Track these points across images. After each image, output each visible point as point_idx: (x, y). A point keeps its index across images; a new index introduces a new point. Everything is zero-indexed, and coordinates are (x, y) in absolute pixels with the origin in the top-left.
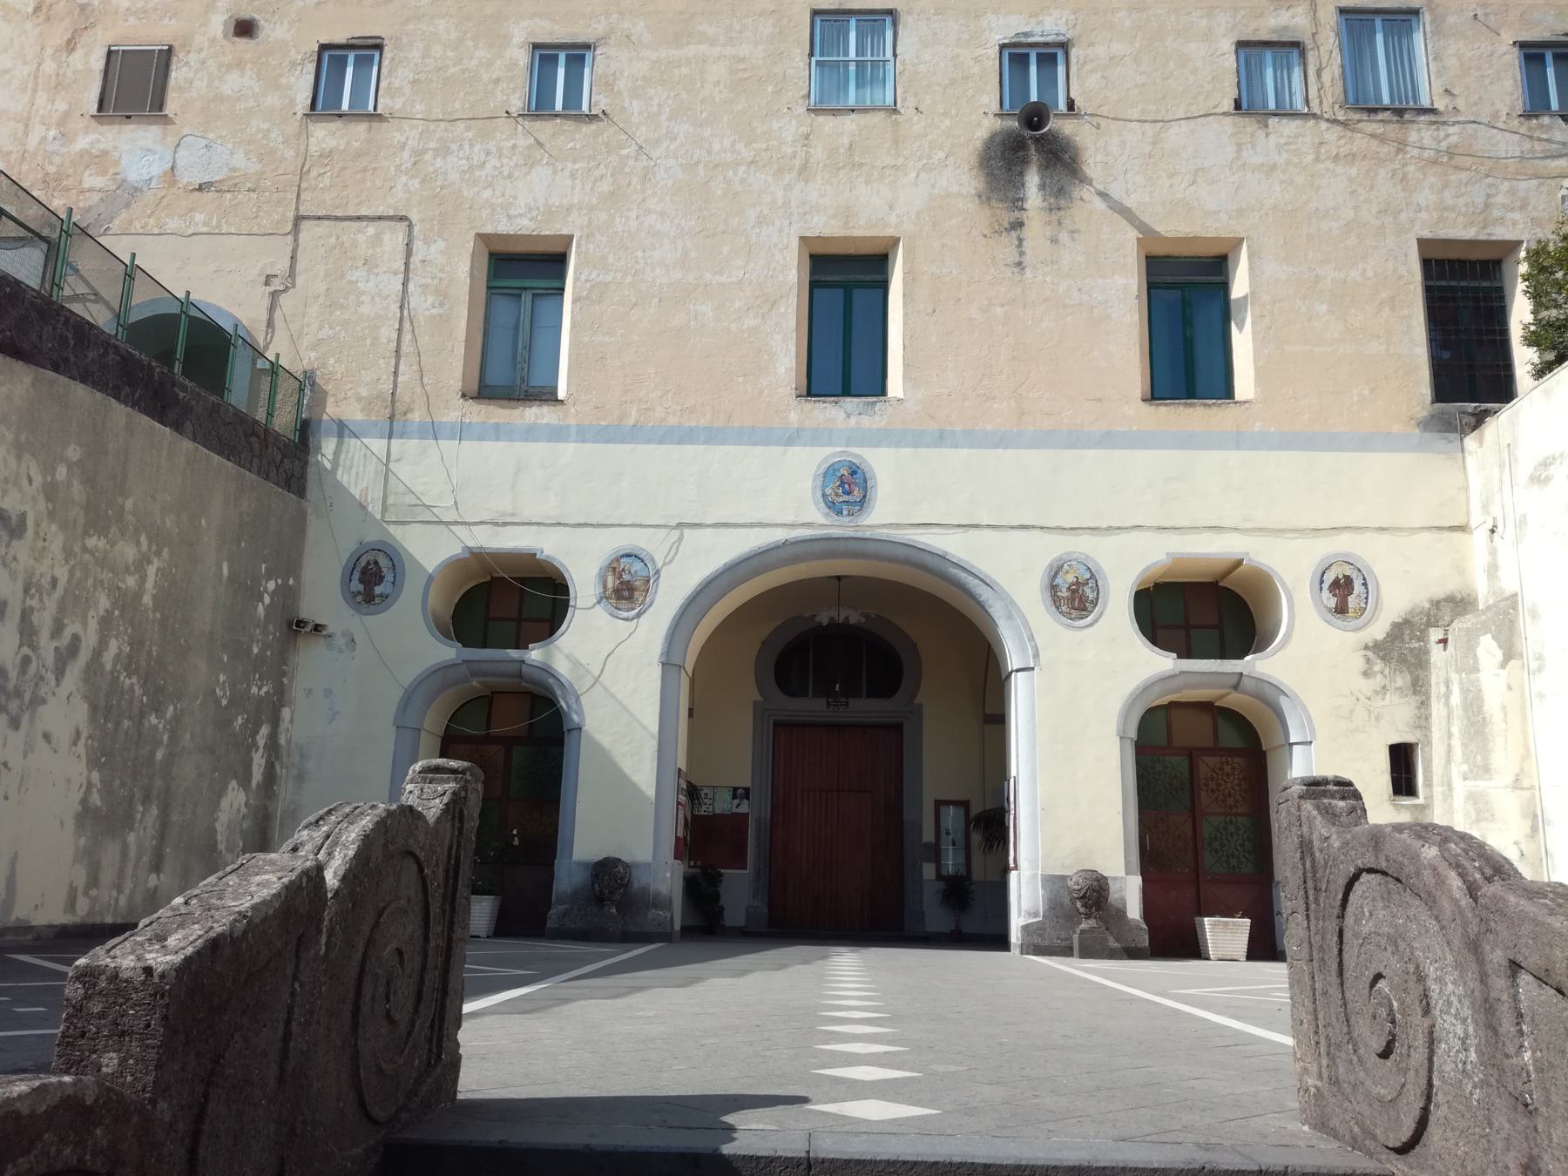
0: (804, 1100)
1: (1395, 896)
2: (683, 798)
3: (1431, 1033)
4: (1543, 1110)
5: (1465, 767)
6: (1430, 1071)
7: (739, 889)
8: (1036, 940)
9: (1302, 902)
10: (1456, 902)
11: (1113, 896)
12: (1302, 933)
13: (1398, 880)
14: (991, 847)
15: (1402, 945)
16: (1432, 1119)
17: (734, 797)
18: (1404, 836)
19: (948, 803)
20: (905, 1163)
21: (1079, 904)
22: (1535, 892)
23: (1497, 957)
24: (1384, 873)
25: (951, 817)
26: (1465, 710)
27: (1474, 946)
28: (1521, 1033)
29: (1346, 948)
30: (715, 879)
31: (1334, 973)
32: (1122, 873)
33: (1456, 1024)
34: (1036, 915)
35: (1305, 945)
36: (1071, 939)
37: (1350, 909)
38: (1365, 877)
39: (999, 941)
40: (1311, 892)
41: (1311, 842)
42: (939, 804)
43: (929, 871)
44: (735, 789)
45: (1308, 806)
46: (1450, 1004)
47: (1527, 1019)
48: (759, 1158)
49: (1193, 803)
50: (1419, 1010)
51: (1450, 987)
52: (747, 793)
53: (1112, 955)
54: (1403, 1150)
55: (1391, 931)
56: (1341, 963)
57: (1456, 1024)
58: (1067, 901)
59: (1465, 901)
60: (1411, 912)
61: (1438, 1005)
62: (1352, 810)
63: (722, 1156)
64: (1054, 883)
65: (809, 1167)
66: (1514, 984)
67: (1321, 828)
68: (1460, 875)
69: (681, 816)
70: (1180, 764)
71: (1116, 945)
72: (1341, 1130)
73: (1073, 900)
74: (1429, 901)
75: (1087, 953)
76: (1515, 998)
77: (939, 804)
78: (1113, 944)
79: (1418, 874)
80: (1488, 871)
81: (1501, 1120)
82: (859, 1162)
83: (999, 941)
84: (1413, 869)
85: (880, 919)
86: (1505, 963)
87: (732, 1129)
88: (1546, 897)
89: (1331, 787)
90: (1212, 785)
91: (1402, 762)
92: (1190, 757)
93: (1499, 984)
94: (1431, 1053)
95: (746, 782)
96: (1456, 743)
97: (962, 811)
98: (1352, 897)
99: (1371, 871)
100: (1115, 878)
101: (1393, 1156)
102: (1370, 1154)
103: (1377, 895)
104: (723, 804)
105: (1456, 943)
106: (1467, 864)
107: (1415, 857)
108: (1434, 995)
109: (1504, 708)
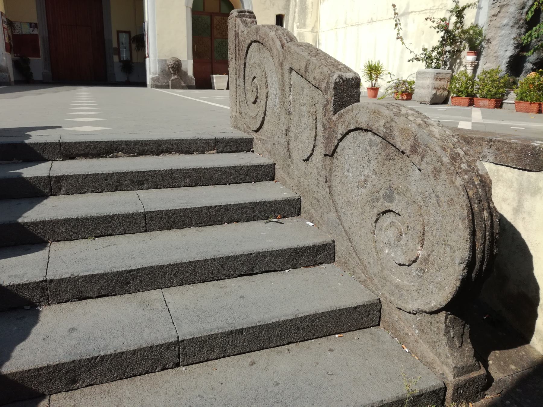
0: (61, 127)
1: (261, 50)
2: (5, 26)
3: (267, 94)
4: (293, 113)
5: (298, 24)
6: (266, 106)
7: (38, 65)
8: (156, 83)
9: (234, 54)
10: (277, 49)
11: (183, 68)
12: (234, 66)
13: (262, 44)
14: (139, 49)
15: (262, 66)
16: (265, 120)
17: (31, 27)
18: (266, 28)
19: (122, 32)
20: (96, 142)
21: (171, 70)
22: (300, 45)
23: (286, 67)
24: (259, 42)
25: (124, 38)
26: (300, 3)
27: (281, 64)
28: (290, 90)
29: (246, 69)
30: (27, 62)
31: (242, 78)
32: (186, 59)
33: (274, 90)
34: (156, 74)
35: (235, 69)
36: (168, 82)
37: (248, 56)
38: (253, 44)
39: (144, 84)
40: (237, 51)
41: (238, 33)
42: (118, 32)
43: (116, 59)
44: (31, 24)
45: (238, 20)
46: (273, 84)
47: (292, 86)
48: (40, 144)
49: (211, 34)
50: (265, 88)
51: (274, 78)
52: (36, 26)
53: (183, 88)
54: (257, 131)
55: (259, 62)
56: (244, 75)
57: (274, 90)
58: (167, 69)
59: (280, 49)
60: (265, 55)
61: (270, 84)
62: (252, 22)
63: (25, 144)
64: (163, 62)
65: (61, 145)
66: (290, 75)
67: (242, 28)
68: (280, 41)
69: (6, 33)
70: (207, 18)
71: (184, 84)
72: (242, 127)
73: (169, 69)
74: (270, 50)
75: (174, 87)
76: (290, 80)
77: (118, 32)
78: (183, 84)
79: (268, 41)
80: (289, 40)
81: (282, 118)
82: (79, 143)
83: (144, 84)
84: (267, 39)
85: (98, 76)
86: (289, 68)
87: (30, 136)
88: (302, 46)
89: (246, 13)
90: (218, 27)
91: (280, 20)
92: (211, 16)
93: (286, 75)
94: (267, 100)
95: (36, 21)
96: (297, 15)
97: (128, 35)
98: (249, 52)
99: (255, 41)
100: (184, 61)
101: (254, 133)
102: (248, 133)
103: (256, 50)
104: (26, 30)
105: (277, 64)
106: (283, 38)
107: (267, 36)
108: (269, 82)
109: (312, 3)
